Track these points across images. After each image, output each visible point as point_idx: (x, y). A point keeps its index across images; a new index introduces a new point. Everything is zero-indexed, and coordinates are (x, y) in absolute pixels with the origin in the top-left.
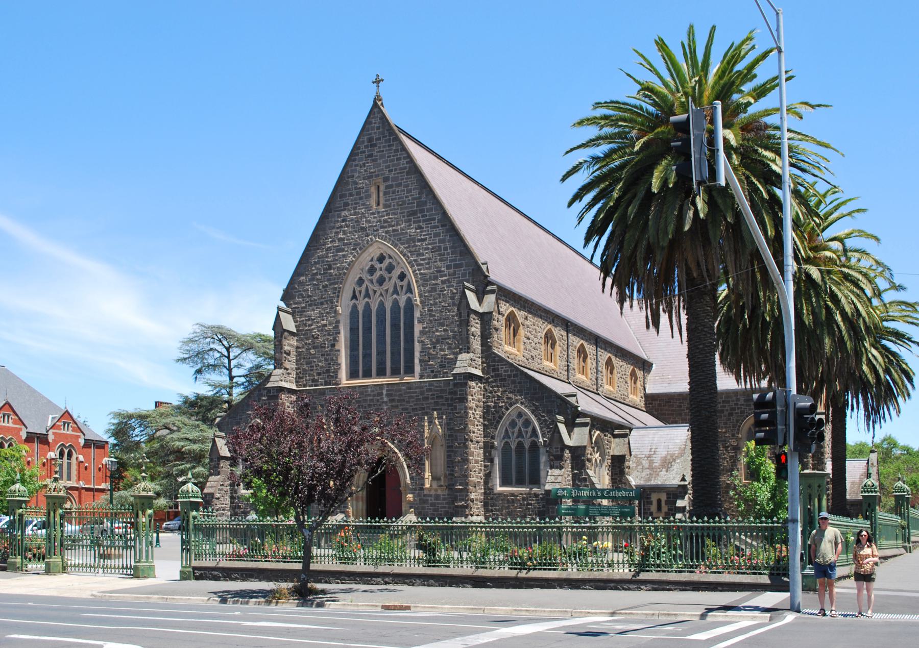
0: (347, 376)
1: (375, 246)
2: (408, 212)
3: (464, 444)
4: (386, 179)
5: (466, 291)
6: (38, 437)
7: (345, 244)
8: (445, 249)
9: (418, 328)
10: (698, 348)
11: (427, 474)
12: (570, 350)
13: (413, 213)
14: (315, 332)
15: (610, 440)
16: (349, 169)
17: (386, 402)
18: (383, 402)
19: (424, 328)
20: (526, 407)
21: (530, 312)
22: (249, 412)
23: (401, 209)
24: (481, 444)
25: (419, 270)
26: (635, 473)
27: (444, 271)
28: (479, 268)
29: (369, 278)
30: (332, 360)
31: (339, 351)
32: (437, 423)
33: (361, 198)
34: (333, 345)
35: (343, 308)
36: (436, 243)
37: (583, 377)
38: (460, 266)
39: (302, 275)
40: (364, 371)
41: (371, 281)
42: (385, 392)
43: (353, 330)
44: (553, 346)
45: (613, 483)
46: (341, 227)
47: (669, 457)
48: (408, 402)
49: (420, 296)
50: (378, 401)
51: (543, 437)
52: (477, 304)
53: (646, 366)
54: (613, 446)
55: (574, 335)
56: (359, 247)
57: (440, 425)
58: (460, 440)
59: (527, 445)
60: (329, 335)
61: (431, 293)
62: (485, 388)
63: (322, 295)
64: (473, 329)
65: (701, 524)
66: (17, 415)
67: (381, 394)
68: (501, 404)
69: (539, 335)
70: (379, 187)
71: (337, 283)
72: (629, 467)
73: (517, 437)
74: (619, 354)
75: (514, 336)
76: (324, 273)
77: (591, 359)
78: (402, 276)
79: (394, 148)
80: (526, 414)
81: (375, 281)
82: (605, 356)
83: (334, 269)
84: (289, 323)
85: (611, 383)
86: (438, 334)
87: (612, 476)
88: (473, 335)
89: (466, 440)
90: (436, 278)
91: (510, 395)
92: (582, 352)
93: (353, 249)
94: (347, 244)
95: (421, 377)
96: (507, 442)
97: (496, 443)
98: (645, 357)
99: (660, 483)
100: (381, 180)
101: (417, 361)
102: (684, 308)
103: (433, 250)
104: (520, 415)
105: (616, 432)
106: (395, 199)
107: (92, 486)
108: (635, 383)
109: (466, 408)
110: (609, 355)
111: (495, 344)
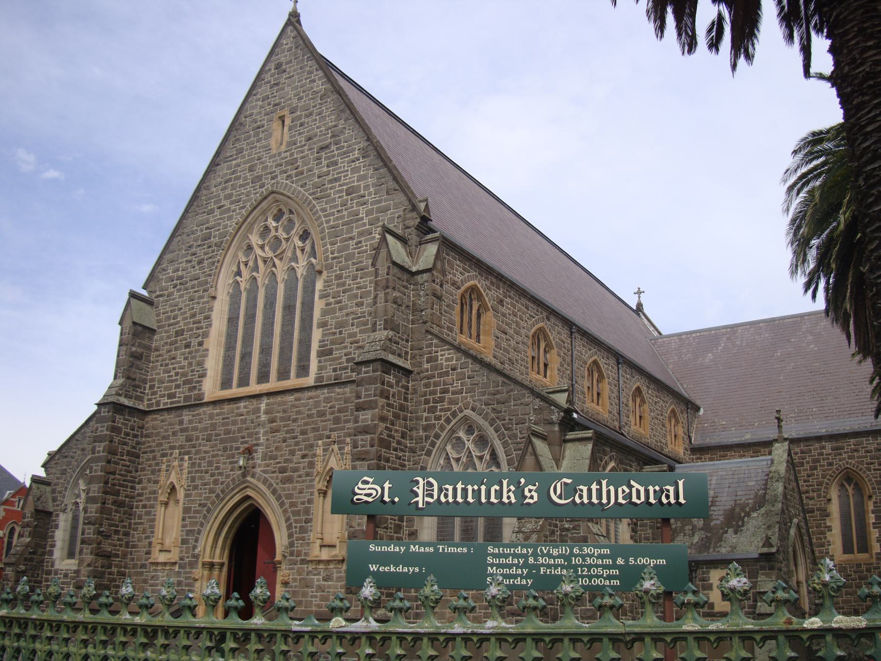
8: (366, 187)
9: (319, 305)
12: (576, 365)
16: (248, 106)
19: (327, 304)
36: (353, 182)
47: (738, 510)
48: (295, 421)
69: (523, 331)
77: (609, 384)
79: (308, 69)
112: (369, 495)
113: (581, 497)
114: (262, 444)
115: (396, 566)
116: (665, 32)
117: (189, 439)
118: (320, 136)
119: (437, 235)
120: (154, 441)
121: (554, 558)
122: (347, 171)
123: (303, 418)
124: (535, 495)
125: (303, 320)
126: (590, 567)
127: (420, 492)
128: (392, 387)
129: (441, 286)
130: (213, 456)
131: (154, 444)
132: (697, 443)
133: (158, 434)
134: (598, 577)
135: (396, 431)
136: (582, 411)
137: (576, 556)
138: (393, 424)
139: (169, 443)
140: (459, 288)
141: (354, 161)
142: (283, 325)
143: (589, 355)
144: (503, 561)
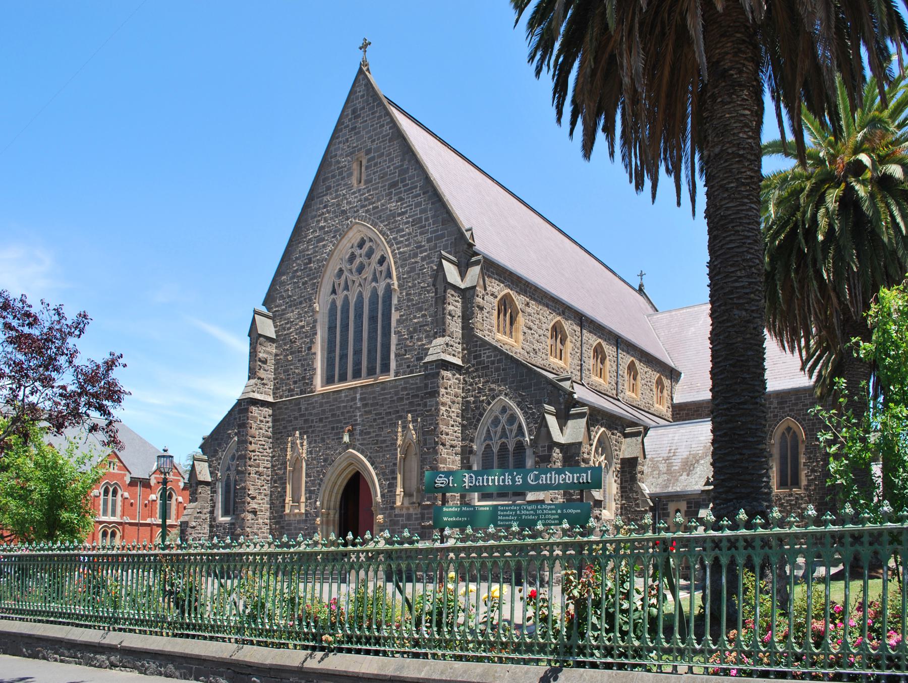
0: (322, 382)
1: (355, 229)
2: (389, 184)
3: (434, 448)
4: (368, 152)
5: (443, 261)
6: (140, 482)
7: (325, 233)
8: (427, 219)
9: (395, 316)
10: (727, 190)
11: (399, 490)
12: (584, 348)
13: (394, 185)
14: (294, 336)
15: (620, 440)
16: (332, 148)
17: (359, 408)
18: (356, 408)
19: (401, 316)
20: (510, 398)
21: (532, 298)
22: (230, 432)
23: (383, 182)
24: (458, 449)
25: (398, 249)
26: (650, 479)
27: (424, 246)
28: (462, 235)
29: (349, 267)
30: (308, 365)
31: (315, 354)
32: (411, 427)
33: (343, 179)
34: (310, 348)
35: (321, 306)
36: (417, 214)
37: (601, 381)
38: (442, 236)
39: (284, 275)
40: (340, 375)
41: (351, 271)
42: (358, 396)
43: (332, 329)
44: (563, 342)
45: (622, 492)
46: (323, 214)
48: (382, 405)
49: (399, 279)
50: (351, 407)
51: (530, 435)
52: (459, 279)
53: (674, 375)
54: (623, 447)
55: (590, 332)
56: (339, 233)
57: (415, 430)
58: (430, 444)
59: (511, 447)
60: (306, 337)
61: (410, 272)
62: (464, 380)
63: (302, 293)
64: (450, 308)
65: (728, 533)
66: (122, 462)
67: (354, 399)
68: (482, 398)
69: (544, 326)
70: (361, 162)
71: (315, 278)
72: (642, 473)
73: (501, 438)
74: (644, 359)
75: (511, 324)
76: (304, 269)
78: (382, 260)
79: (377, 114)
80: (511, 409)
81: (354, 270)
82: (626, 359)
83: (314, 262)
84: (267, 328)
85: (633, 389)
86: (416, 321)
87: (621, 483)
88: (450, 315)
89: (437, 443)
90: (415, 256)
91: (493, 386)
92: (599, 352)
93: (333, 237)
94: (328, 232)
95: (397, 374)
96: (488, 445)
97: (475, 447)
98: (672, 365)
99: (679, 490)
100: (363, 154)
101: (392, 356)
102: (701, 170)
103: (414, 223)
104: (504, 410)
105: (628, 430)
106: (377, 172)
107: (137, 521)
108: (662, 392)
109: (437, 403)
110: (632, 358)
111: (479, 325)
112: (442, 483)
113: (542, 480)
114: (359, 424)
115: (456, 517)
116: (615, 157)
117: (306, 421)
118: (390, 175)
119: (479, 257)
120: (281, 425)
121: (529, 511)
122: (412, 205)
123: (387, 404)
124: (521, 480)
125: (383, 328)
126: (545, 514)
127: (467, 481)
128: (449, 379)
129: (483, 299)
130: (325, 434)
131: (281, 427)
132: (678, 402)
133: (283, 419)
134: (549, 519)
135: (453, 412)
136: (588, 384)
137: (539, 509)
138: (450, 408)
139: (292, 425)
140: (496, 297)
141: (416, 197)
142: (369, 332)
143: (593, 340)
144: (505, 513)
